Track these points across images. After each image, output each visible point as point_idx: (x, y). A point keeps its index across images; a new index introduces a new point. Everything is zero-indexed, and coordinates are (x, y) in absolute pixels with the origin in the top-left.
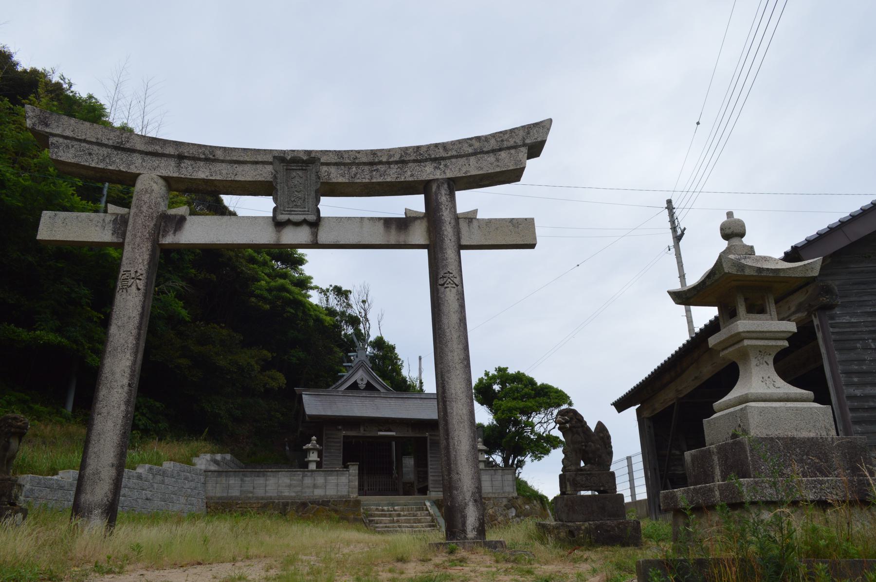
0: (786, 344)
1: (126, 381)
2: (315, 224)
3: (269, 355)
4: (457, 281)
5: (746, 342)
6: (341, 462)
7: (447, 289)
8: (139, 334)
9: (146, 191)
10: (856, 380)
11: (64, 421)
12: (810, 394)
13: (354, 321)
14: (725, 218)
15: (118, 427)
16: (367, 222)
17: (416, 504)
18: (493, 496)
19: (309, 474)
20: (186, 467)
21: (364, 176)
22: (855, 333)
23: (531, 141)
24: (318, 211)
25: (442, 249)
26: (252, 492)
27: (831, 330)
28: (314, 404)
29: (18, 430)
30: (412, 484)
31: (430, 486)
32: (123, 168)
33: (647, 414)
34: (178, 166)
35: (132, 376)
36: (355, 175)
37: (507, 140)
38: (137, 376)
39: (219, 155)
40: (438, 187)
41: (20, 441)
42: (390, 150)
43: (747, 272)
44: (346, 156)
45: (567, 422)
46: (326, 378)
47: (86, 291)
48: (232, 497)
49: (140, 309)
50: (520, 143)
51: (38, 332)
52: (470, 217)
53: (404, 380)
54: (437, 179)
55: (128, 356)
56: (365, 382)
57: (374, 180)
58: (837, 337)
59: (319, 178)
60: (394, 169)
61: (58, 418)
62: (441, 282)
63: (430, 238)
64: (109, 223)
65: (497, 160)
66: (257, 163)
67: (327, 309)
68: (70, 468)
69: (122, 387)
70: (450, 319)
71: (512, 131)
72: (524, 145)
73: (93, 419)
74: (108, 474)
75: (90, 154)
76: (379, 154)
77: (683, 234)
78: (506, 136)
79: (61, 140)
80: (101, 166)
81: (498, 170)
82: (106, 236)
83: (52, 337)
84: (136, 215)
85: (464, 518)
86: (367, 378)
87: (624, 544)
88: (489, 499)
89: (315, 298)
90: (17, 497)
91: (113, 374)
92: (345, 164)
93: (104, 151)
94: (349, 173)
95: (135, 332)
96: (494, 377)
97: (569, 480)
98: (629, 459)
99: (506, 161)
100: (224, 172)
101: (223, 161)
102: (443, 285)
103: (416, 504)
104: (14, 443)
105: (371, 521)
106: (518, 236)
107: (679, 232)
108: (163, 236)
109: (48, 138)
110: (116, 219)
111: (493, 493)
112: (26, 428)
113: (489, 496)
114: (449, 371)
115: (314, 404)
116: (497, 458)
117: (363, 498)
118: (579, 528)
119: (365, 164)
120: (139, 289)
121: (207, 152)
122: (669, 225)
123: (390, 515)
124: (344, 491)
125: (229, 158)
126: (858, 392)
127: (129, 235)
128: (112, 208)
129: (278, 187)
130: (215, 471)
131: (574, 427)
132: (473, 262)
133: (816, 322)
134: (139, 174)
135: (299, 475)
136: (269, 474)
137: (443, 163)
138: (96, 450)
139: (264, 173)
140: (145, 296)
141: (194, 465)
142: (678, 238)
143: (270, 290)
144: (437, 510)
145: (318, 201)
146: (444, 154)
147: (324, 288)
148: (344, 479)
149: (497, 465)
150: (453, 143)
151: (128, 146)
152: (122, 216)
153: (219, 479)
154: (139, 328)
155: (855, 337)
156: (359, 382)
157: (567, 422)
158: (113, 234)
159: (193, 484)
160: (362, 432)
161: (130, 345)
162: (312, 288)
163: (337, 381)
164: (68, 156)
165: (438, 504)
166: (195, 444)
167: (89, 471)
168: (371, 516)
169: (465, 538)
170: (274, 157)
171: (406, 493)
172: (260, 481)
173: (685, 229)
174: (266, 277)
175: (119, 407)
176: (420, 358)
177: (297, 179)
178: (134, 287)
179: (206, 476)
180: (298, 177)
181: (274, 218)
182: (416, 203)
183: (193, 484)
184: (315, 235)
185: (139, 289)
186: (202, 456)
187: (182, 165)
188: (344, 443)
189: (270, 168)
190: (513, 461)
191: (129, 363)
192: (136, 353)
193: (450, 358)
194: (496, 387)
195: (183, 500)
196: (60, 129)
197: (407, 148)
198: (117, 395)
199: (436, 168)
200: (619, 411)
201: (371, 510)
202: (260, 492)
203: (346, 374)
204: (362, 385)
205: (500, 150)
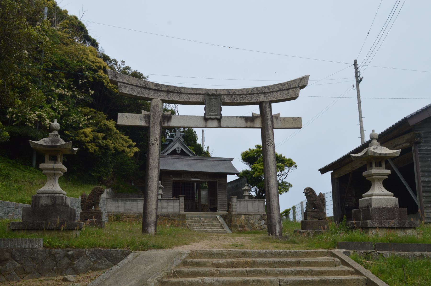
0: (387, 177)
4: (272, 143)
5: (374, 177)
6: (172, 194)
10: (426, 174)
12: (392, 194)
14: (371, 132)
16: (238, 118)
18: (253, 213)
22: (428, 154)
23: (301, 83)
24: (221, 114)
26: (131, 210)
27: (419, 152)
30: (205, 206)
32: (147, 96)
33: (336, 176)
37: (292, 85)
39: (183, 91)
42: (247, 89)
43: (376, 155)
44: (230, 91)
45: (308, 193)
48: (120, 212)
50: (297, 86)
52: (277, 117)
56: (180, 149)
58: (421, 156)
60: (249, 97)
62: (267, 143)
65: (288, 93)
66: (196, 94)
71: (294, 81)
75: (134, 90)
77: (361, 80)
78: (292, 83)
79: (122, 84)
80: (139, 95)
82: (142, 123)
84: (154, 116)
86: (181, 147)
88: (251, 215)
91: (153, 177)
92: (230, 95)
93: (139, 89)
94: (232, 98)
100: (185, 98)
101: (184, 93)
103: (212, 217)
106: (295, 123)
107: (359, 79)
113: (251, 214)
114: (270, 177)
117: (189, 214)
119: (238, 95)
121: (178, 90)
122: (354, 74)
123: (199, 222)
124: (177, 210)
126: (427, 179)
128: (143, 112)
133: (413, 148)
134: (153, 99)
136: (138, 200)
139: (200, 98)
142: (359, 82)
146: (268, 91)
148: (177, 204)
150: (271, 86)
151: (148, 87)
152: (148, 115)
155: (428, 155)
156: (177, 149)
157: (308, 193)
160: (182, 179)
164: (126, 91)
165: (224, 217)
172: (135, 204)
173: (362, 78)
177: (213, 102)
182: (255, 109)
189: (201, 96)
191: (157, 173)
197: (254, 88)
198: (155, 184)
199: (265, 96)
200: (322, 174)
204: (179, 151)
205: (290, 89)
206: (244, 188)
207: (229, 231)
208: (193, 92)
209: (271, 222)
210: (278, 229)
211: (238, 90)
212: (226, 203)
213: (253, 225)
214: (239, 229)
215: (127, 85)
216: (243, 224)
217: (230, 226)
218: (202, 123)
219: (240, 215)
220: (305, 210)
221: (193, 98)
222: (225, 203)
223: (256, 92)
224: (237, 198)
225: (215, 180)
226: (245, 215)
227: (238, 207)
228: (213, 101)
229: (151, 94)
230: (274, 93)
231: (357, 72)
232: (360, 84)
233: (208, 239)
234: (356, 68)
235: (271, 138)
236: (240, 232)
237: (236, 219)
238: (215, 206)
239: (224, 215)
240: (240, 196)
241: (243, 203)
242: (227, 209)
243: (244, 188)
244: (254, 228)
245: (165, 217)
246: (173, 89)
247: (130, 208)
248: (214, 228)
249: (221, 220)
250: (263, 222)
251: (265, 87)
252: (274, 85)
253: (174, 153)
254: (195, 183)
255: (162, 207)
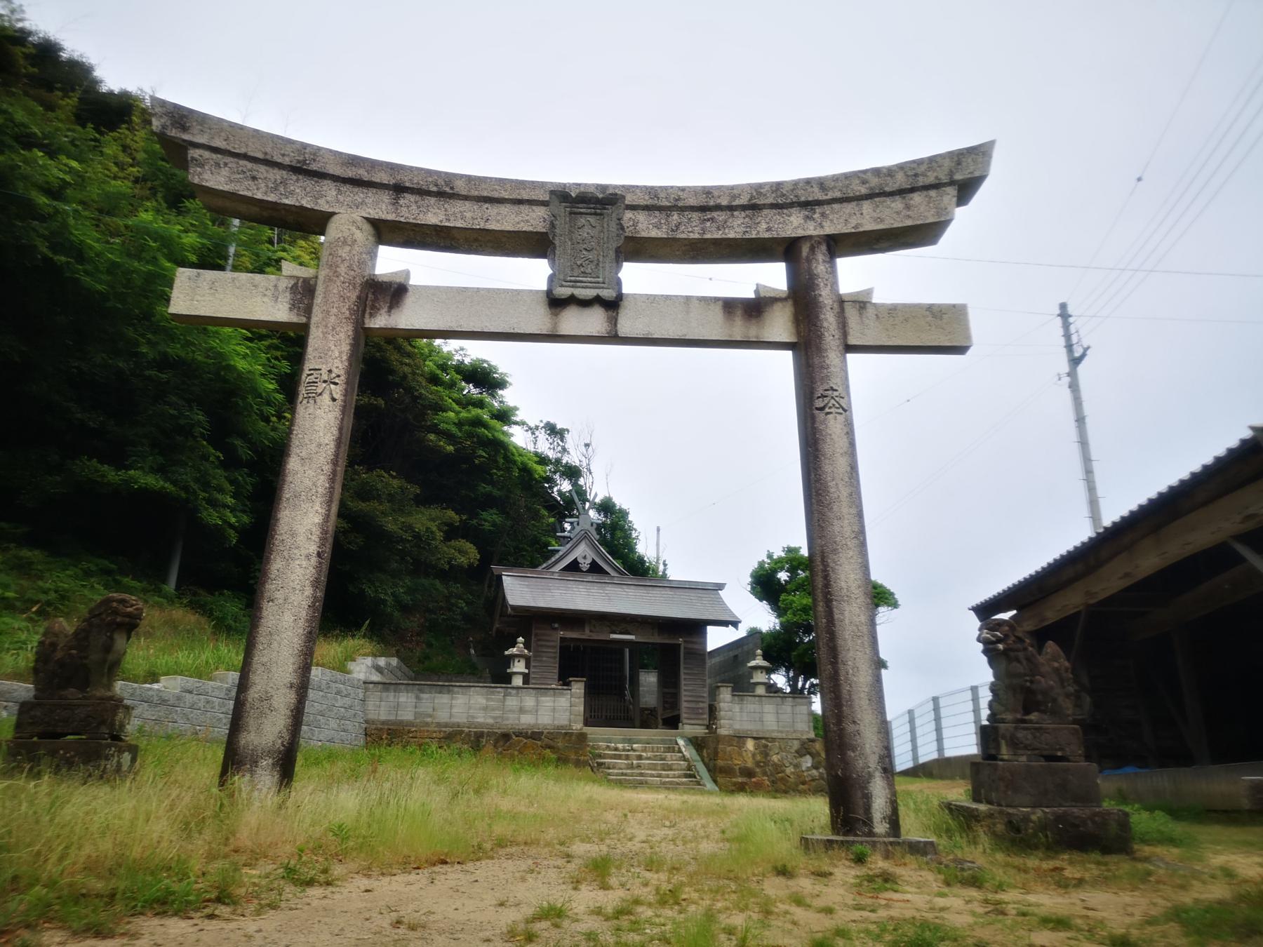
1: (313, 549)
2: (612, 305)
3: (457, 517)
7: (830, 416)
8: (334, 473)
9: (345, 242)
11: (164, 601)
13: (572, 473)
15: (302, 623)
17: (663, 742)
18: (780, 735)
19: (514, 692)
20: (338, 675)
21: (692, 229)
23: (959, 176)
25: (820, 350)
26: (430, 716)
28: (519, 590)
29: (127, 620)
30: (652, 711)
31: (684, 715)
32: (307, 203)
34: (395, 203)
35: (323, 540)
36: (677, 227)
37: (924, 175)
38: (331, 540)
39: (461, 188)
40: (812, 249)
41: (128, 639)
42: (732, 188)
44: (662, 195)
45: (999, 641)
46: (533, 555)
47: (201, 417)
48: (401, 722)
49: (336, 432)
51: (132, 472)
52: (861, 303)
53: (641, 560)
54: (810, 237)
55: (317, 507)
56: (589, 561)
57: (708, 236)
59: (622, 228)
61: (156, 598)
62: (819, 403)
63: (798, 333)
64: (284, 292)
65: (908, 207)
66: (519, 202)
67: (536, 454)
68: (176, 673)
69: (308, 557)
70: (835, 467)
71: (932, 160)
72: (952, 183)
73: (260, 609)
74: (283, 700)
76: (716, 194)
79: (207, 154)
81: (909, 223)
82: (280, 312)
83: (152, 481)
84: (329, 280)
85: (868, 798)
86: (591, 555)
87: (1106, 850)
88: (773, 740)
89: (518, 438)
90: (122, 726)
91: (293, 535)
93: (277, 174)
95: (328, 468)
96: (780, 560)
97: (1004, 737)
98: (974, 689)
99: (920, 209)
100: (468, 215)
101: (466, 198)
102: (822, 409)
103: (663, 742)
104: (120, 641)
105: (600, 765)
106: (936, 332)
108: (371, 315)
109: (186, 149)
110: (296, 285)
111: (779, 731)
112: (139, 617)
113: (774, 735)
114: (835, 551)
115: (519, 590)
116: (780, 679)
117: (595, 733)
118: (1026, 819)
119: (693, 209)
120: (334, 400)
121: (441, 182)
122: (1062, 341)
123: (627, 757)
124: (562, 719)
125: (476, 193)
127: (317, 311)
129: (557, 242)
130: (379, 683)
131: (1011, 650)
132: (866, 378)
135: (499, 692)
136: (456, 689)
137: (818, 210)
138: (265, 659)
139: (533, 220)
140: (344, 410)
141: (349, 672)
142: (1075, 362)
143: (460, 424)
144: (694, 752)
145: (619, 267)
147: (532, 425)
149: (780, 690)
150: (836, 178)
151: (314, 167)
153: (384, 694)
154: (335, 463)
157: (999, 641)
158: (291, 309)
159: (347, 701)
160: (587, 634)
161: (320, 490)
162: (516, 423)
163: (548, 558)
166: (351, 643)
167: (253, 694)
168: (600, 756)
169: (871, 833)
170: (552, 192)
171: (645, 725)
172: (443, 699)
174: (454, 405)
175: (302, 591)
176: (658, 530)
178: (326, 397)
179: (366, 690)
180: (588, 226)
181: (549, 293)
183: (347, 701)
184: (613, 322)
185: (334, 400)
186: (360, 660)
187: (401, 202)
188: (561, 647)
189: (541, 212)
190: (804, 685)
191: (318, 519)
192: (329, 503)
193: (837, 529)
194: (783, 576)
195: (333, 724)
196: (206, 136)
197: (760, 186)
198: (299, 571)
199: (807, 218)
201: (599, 748)
202: (443, 716)
203: (563, 549)
204: (585, 565)
205: (913, 190)
206: (752, 663)
207: (710, 785)
208: (505, 195)
209: (846, 764)
210: (879, 805)
211: (695, 191)
212: (706, 705)
213: (779, 768)
214: (740, 780)
215: (229, 159)
216: (750, 764)
217: (714, 772)
218: (539, 320)
219: (740, 738)
220: (985, 713)
221: (505, 220)
222: (701, 705)
223: (770, 200)
224: (733, 690)
225: (673, 641)
226: (755, 738)
227: (737, 715)
228: (587, 240)
229: (325, 198)
230: (849, 208)
231: (1067, 336)
232: (1081, 368)
233: (647, 807)
234: (1066, 326)
235: (835, 382)
236: (741, 789)
237: (729, 749)
238: (676, 713)
239: (696, 738)
240: (742, 686)
241: (751, 705)
242: (706, 722)
243: (752, 663)
244: (782, 779)
245: (527, 737)
246: (417, 181)
247: (430, 711)
248: (668, 776)
249: (689, 752)
250: (807, 762)
251: (808, 182)
252: (847, 176)
253: (574, 567)
254: (627, 651)
255: (522, 710)
